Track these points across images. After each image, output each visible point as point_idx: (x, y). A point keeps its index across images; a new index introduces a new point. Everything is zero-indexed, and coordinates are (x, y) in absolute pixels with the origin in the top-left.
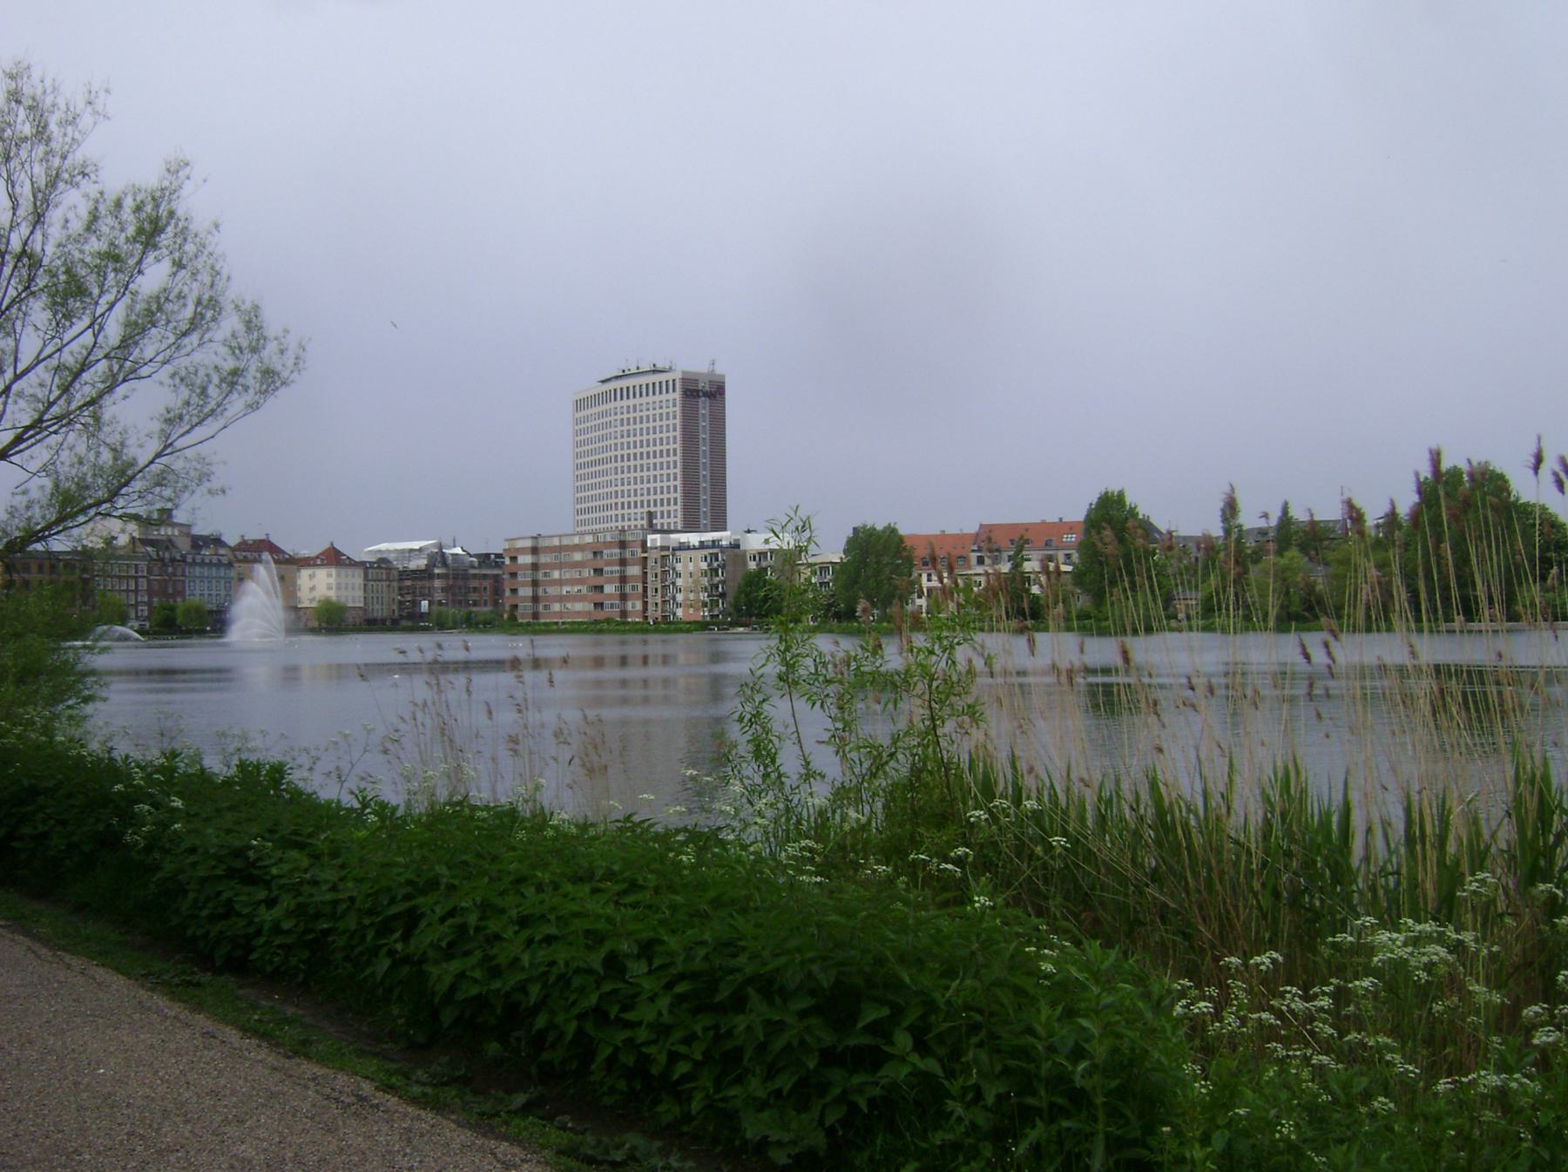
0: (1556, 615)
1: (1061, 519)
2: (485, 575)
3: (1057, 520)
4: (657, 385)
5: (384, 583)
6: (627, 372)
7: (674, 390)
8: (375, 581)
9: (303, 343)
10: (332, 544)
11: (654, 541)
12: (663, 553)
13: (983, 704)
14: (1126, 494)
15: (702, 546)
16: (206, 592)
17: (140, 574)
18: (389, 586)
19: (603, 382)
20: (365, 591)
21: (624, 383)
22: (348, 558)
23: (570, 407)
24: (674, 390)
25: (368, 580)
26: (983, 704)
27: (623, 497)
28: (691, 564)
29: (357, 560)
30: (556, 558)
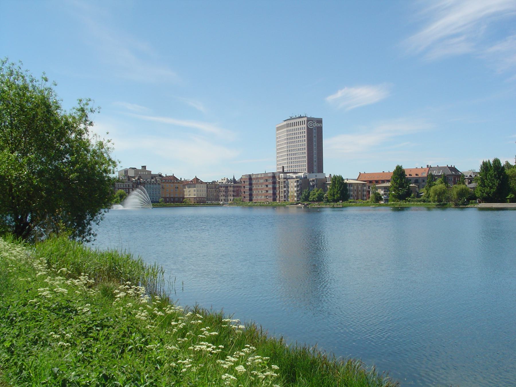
0: (512, 201)
1: (438, 166)
2: (237, 186)
3: (436, 166)
4: (294, 123)
5: (214, 189)
6: (292, 118)
7: (304, 124)
8: (210, 188)
9: (87, 108)
10: (196, 176)
11: (282, 176)
12: (284, 180)
13: (108, 249)
14: (142, 165)
15: (297, 177)
16: (152, 193)
17: (130, 187)
18: (216, 190)
19: (285, 121)
20: (207, 192)
21: (292, 121)
22: (201, 181)
23: (275, 129)
24: (304, 124)
25: (208, 188)
26: (108, 249)
27: (303, 161)
28: (292, 184)
29: (204, 182)
30: (259, 181)
